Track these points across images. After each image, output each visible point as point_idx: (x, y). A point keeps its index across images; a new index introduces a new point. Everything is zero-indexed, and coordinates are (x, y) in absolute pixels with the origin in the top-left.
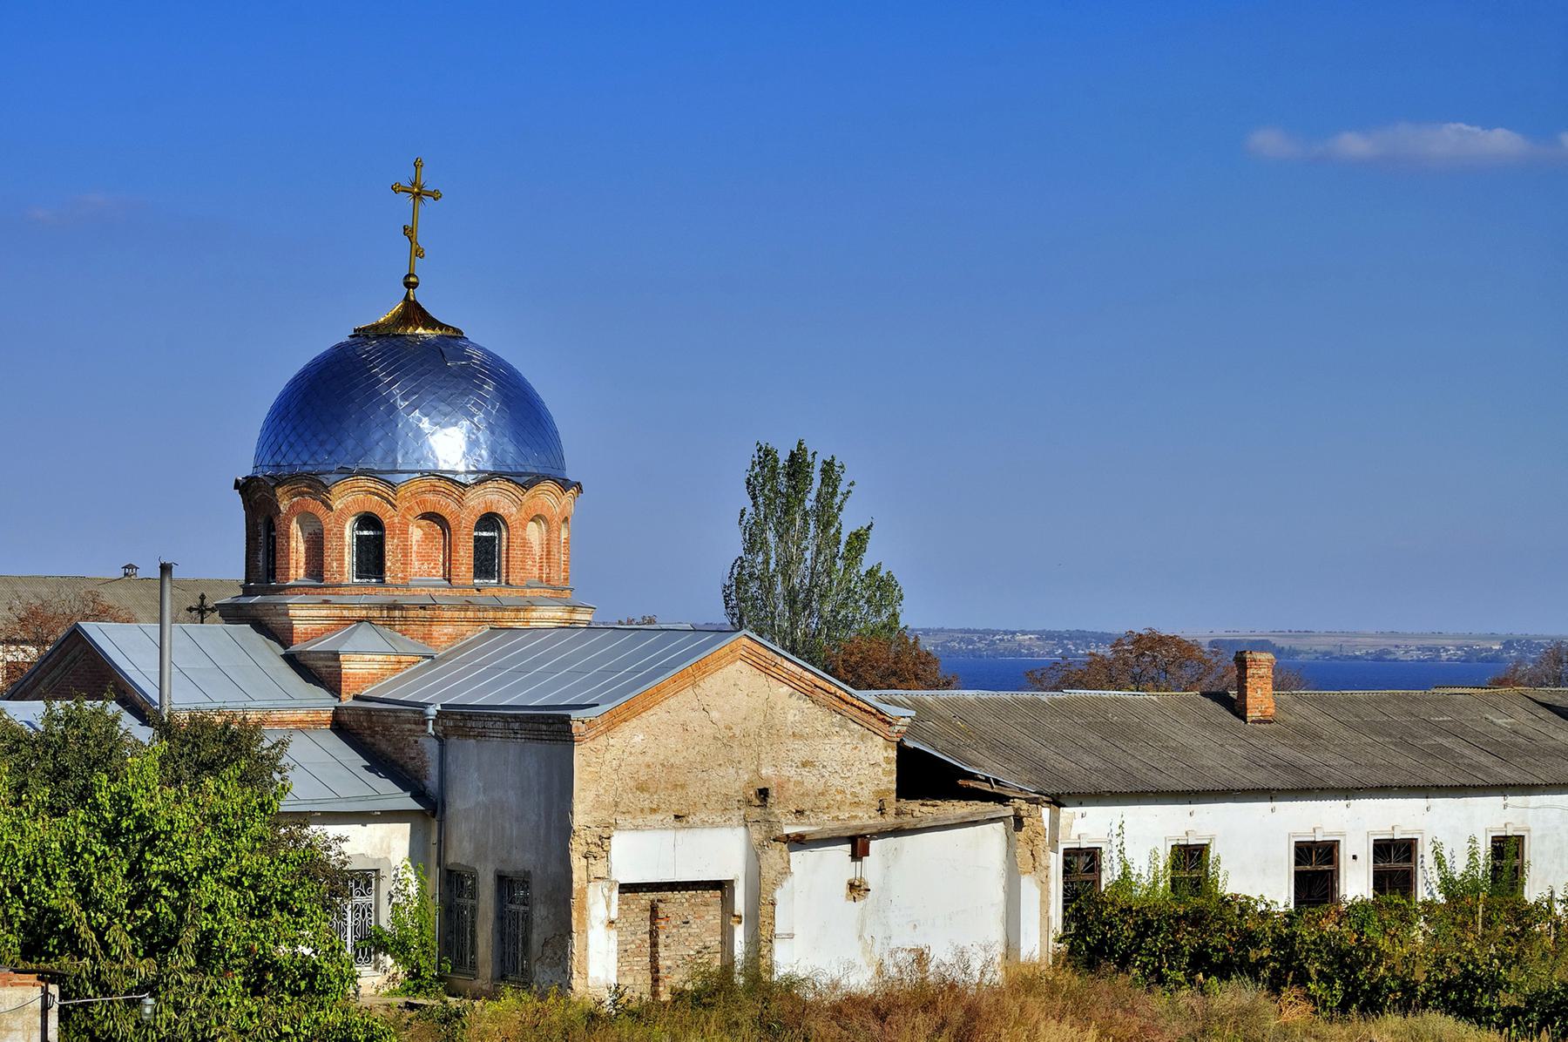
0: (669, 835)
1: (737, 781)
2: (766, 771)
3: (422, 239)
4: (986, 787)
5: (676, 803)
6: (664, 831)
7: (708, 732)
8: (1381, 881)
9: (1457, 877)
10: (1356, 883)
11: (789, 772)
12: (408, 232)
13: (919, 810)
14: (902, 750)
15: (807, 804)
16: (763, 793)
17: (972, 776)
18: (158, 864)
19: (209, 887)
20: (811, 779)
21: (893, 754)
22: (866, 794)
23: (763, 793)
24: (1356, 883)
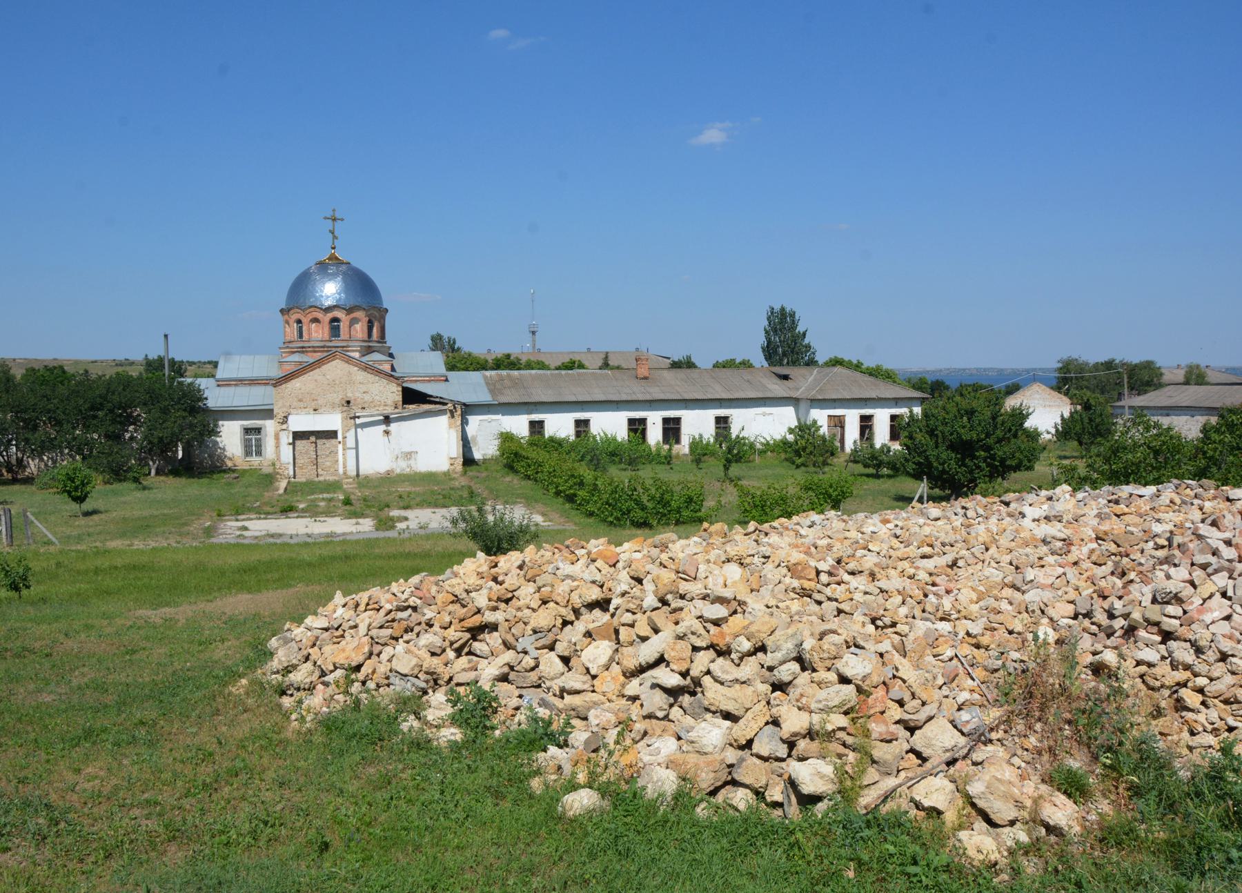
0: (311, 417)
1: (337, 397)
2: (349, 395)
3: (336, 233)
4: (438, 400)
5: (314, 405)
6: (678, 370)
7: (326, 382)
8: (666, 432)
9: (1027, 424)
10: (654, 434)
11: (357, 395)
12: (332, 232)
13: (412, 408)
14: (403, 388)
15: (366, 406)
16: (348, 402)
17: (431, 396)
18: (1113, 797)
19: (645, 499)
20: (367, 398)
21: (400, 389)
22: (389, 402)
23: (348, 402)
24: (654, 434)
